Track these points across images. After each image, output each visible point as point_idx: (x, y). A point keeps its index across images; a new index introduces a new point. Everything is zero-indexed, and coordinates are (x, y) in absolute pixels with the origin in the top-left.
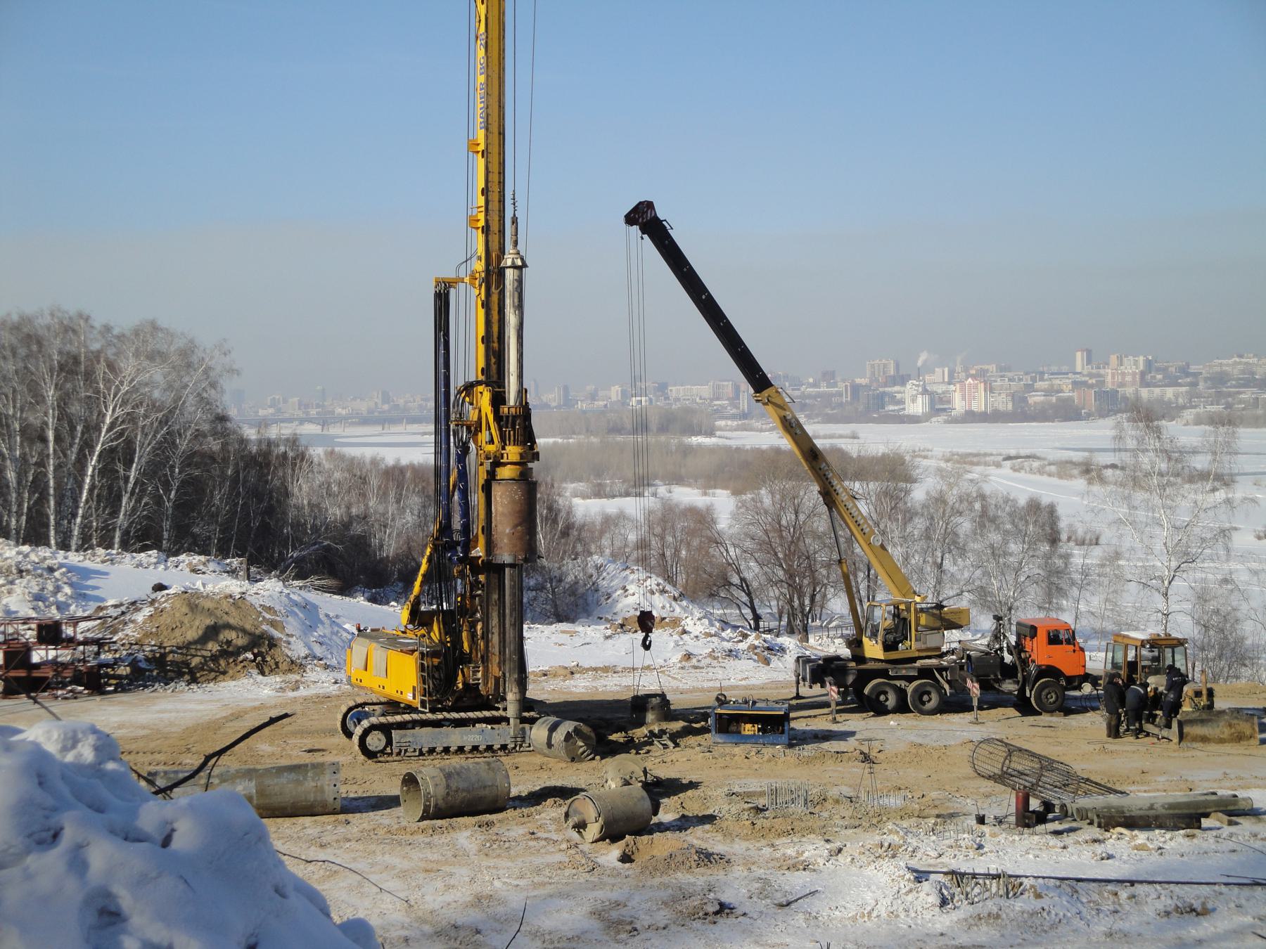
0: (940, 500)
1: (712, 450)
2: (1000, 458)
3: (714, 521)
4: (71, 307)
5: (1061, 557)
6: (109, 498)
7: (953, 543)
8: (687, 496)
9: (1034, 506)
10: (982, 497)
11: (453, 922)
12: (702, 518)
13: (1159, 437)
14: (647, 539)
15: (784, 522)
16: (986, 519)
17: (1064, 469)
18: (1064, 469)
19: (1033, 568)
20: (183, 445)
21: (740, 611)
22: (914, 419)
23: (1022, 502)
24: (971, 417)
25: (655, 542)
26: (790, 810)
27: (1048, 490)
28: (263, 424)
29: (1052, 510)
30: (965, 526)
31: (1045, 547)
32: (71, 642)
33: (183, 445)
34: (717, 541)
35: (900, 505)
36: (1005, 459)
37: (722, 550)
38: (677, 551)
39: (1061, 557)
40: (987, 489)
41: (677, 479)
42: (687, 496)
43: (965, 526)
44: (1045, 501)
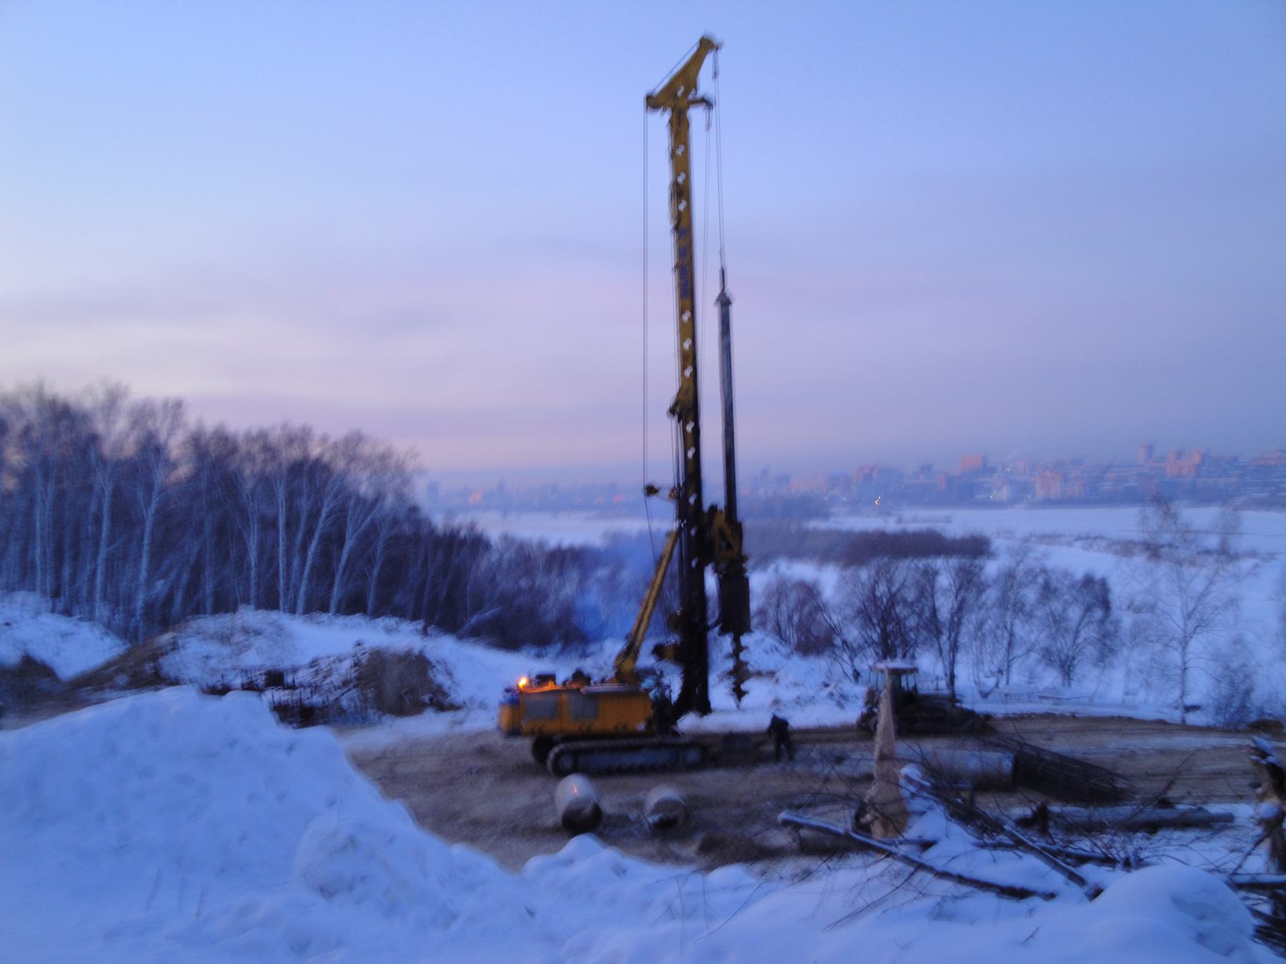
0: (1010, 575)
1: (829, 533)
2: (1072, 539)
3: (819, 594)
4: (297, 423)
5: (1111, 623)
6: (324, 571)
7: (1019, 608)
8: (803, 571)
9: (1088, 581)
10: (1044, 571)
11: (437, 659)
12: (809, 591)
13: (1175, 523)
14: (866, 636)
15: (878, 594)
16: (1048, 591)
17: (1125, 548)
18: (1125, 548)
19: (1089, 633)
20: (384, 533)
21: (1216, 796)
22: (999, 505)
23: (1079, 575)
24: (1048, 503)
25: (771, 612)
26: (324, 478)
27: (1100, 563)
28: (450, 513)
29: (1104, 584)
30: (1030, 595)
31: (1098, 613)
32: (293, 687)
33: (384, 533)
34: (820, 608)
35: (975, 579)
36: (1076, 540)
37: (826, 617)
38: (790, 618)
39: (1111, 623)
40: (1050, 564)
41: (795, 554)
42: (803, 571)
43: (1030, 595)
44: (1098, 575)
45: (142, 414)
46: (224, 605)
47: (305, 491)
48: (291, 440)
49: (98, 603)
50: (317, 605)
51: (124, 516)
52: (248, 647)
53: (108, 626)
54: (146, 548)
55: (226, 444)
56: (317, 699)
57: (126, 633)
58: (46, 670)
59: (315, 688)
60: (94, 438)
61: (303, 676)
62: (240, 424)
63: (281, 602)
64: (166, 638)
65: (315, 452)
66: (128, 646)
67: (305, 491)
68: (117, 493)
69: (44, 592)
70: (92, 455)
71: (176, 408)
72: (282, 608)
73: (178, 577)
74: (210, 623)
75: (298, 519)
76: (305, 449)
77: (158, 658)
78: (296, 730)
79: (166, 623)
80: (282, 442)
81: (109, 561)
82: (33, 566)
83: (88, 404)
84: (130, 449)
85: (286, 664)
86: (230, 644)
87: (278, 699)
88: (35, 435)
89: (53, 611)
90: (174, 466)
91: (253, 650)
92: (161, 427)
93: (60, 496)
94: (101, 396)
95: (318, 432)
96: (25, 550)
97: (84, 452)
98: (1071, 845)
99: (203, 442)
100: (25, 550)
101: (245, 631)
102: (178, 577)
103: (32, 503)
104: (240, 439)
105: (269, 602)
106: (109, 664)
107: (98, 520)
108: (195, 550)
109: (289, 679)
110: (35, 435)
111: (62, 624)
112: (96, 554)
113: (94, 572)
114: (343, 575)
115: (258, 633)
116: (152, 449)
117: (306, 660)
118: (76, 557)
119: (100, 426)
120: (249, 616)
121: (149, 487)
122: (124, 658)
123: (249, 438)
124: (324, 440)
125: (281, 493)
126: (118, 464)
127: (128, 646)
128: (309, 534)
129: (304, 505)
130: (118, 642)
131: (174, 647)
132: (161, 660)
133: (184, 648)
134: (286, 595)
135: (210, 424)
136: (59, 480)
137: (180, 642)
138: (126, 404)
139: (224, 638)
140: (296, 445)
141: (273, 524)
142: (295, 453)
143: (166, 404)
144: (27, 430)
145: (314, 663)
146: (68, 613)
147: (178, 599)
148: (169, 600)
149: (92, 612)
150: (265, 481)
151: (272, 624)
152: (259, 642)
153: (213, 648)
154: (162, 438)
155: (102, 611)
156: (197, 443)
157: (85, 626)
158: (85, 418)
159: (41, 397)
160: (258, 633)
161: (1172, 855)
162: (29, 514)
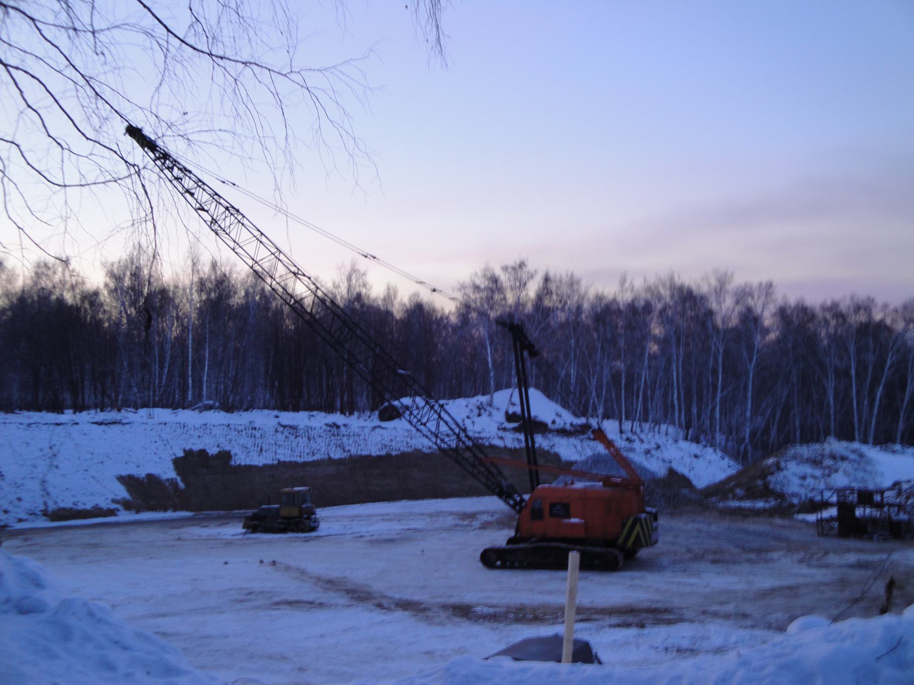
4: (862, 294)
6: (890, 410)
32: (880, 506)
45: (743, 294)
46: (811, 436)
47: (871, 346)
48: (858, 308)
49: (718, 435)
50: (884, 440)
51: (733, 370)
52: (836, 471)
53: (725, 450)
54: (750, 394)
55: (803, 311)
56: (903, 516)
57: (736, 454)
58: (685, 481)
59: (900, 507)
60: (710, 313)
61: (890, 496)
62: (815, 300)
63: (856, 434)
64: (771, 461)
65: (878, 316)
66: (739, 467)
67: (871, 346)
68: (726, 353)
69: (680, 425)
70: (709, 324)
71: (768, 289)
72: (857, 438)
73: (773, 414)
74: (805, 451)
75: (866, 368)
76: (870, 315)
77: (766, 476)
78: (349, 418)
79: (768, 450)
80: (852, 310)
81: (723, 402)
82: (673, 406)
83: (704, 289)
84: (734, 322)
85: (871, 487)
86: (822, 467)
87: (869, 514)
88: (670, 312)
89: (686, 438)
90: (767, 331)
91: (840, 473)
92: (757, 304)
93: (688, 356)
94: (714, 282)
95: (880, 301)
96: (665, 395)
97: (704, 324)
98: (137, 288)
99: (789, 312)
100: (665, 395)
101: (833, 457)
102: (773, 414)
103: (669, 361)
104: (818, 310)
105: (846, 434)
106: (730, 479)
107: (715, 372)
108: (785, 395)
109: (877, 498)
110: (670, 312)
111: (694, 448)
112: (714, 398)
113: (714, 409)
114: (905, 412)
115: (843, 459)
116: (750, 319)
117: (887, 483)
118: (700, 399)
119: (714, 306)
120: (835, 445)
121: (750, 347)
122: (740, 474)
123: (824, 308)
124: (885, 306)
125: (852, 349)
126: (727, 331)
127: (739, 467)
128: (876, 381)
129: (871, 358)
130: (732, 463)
131: (779, 468)
132: (769, 478)
133: (787, 470)
134: (859, 429)
135: (792, 300)
136: (687, 345)
137: (783, 464)
138: (732, 286)
139: (816, 462)
140: (862, 311)
141: (847, 374)
142: (862, 318)
143: (760, 285)
144: (663, 311)
145: (897, 484)
146: (696, 440)
147: (773, 432)
148: (767, 431)
149: (713, 438)
150: (836, 339)
151: (854, 451)
152: (844, 465)
153: (807, 469)
154: (758, 310)
155: (719, 438)
156: (783, 313)
157: (710, 450)
158: (703, 298)
159: (673, 287)
160: (843, 459)
161: (249, 223)
162: (667, 370)
